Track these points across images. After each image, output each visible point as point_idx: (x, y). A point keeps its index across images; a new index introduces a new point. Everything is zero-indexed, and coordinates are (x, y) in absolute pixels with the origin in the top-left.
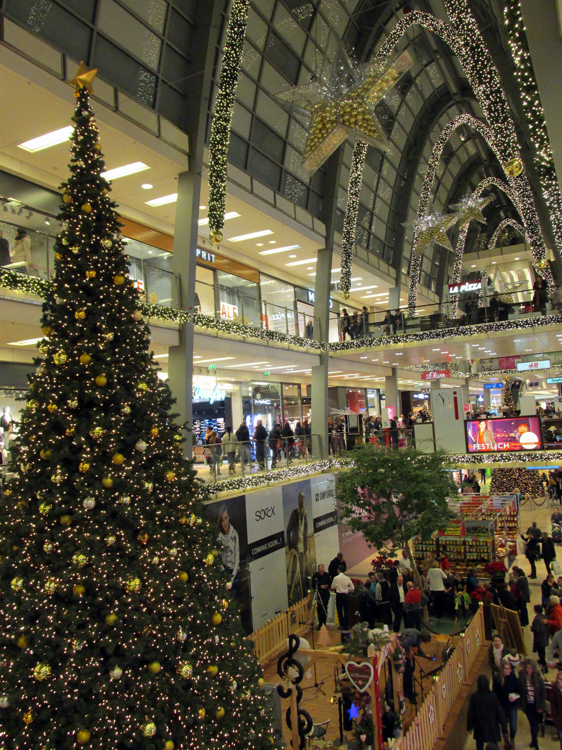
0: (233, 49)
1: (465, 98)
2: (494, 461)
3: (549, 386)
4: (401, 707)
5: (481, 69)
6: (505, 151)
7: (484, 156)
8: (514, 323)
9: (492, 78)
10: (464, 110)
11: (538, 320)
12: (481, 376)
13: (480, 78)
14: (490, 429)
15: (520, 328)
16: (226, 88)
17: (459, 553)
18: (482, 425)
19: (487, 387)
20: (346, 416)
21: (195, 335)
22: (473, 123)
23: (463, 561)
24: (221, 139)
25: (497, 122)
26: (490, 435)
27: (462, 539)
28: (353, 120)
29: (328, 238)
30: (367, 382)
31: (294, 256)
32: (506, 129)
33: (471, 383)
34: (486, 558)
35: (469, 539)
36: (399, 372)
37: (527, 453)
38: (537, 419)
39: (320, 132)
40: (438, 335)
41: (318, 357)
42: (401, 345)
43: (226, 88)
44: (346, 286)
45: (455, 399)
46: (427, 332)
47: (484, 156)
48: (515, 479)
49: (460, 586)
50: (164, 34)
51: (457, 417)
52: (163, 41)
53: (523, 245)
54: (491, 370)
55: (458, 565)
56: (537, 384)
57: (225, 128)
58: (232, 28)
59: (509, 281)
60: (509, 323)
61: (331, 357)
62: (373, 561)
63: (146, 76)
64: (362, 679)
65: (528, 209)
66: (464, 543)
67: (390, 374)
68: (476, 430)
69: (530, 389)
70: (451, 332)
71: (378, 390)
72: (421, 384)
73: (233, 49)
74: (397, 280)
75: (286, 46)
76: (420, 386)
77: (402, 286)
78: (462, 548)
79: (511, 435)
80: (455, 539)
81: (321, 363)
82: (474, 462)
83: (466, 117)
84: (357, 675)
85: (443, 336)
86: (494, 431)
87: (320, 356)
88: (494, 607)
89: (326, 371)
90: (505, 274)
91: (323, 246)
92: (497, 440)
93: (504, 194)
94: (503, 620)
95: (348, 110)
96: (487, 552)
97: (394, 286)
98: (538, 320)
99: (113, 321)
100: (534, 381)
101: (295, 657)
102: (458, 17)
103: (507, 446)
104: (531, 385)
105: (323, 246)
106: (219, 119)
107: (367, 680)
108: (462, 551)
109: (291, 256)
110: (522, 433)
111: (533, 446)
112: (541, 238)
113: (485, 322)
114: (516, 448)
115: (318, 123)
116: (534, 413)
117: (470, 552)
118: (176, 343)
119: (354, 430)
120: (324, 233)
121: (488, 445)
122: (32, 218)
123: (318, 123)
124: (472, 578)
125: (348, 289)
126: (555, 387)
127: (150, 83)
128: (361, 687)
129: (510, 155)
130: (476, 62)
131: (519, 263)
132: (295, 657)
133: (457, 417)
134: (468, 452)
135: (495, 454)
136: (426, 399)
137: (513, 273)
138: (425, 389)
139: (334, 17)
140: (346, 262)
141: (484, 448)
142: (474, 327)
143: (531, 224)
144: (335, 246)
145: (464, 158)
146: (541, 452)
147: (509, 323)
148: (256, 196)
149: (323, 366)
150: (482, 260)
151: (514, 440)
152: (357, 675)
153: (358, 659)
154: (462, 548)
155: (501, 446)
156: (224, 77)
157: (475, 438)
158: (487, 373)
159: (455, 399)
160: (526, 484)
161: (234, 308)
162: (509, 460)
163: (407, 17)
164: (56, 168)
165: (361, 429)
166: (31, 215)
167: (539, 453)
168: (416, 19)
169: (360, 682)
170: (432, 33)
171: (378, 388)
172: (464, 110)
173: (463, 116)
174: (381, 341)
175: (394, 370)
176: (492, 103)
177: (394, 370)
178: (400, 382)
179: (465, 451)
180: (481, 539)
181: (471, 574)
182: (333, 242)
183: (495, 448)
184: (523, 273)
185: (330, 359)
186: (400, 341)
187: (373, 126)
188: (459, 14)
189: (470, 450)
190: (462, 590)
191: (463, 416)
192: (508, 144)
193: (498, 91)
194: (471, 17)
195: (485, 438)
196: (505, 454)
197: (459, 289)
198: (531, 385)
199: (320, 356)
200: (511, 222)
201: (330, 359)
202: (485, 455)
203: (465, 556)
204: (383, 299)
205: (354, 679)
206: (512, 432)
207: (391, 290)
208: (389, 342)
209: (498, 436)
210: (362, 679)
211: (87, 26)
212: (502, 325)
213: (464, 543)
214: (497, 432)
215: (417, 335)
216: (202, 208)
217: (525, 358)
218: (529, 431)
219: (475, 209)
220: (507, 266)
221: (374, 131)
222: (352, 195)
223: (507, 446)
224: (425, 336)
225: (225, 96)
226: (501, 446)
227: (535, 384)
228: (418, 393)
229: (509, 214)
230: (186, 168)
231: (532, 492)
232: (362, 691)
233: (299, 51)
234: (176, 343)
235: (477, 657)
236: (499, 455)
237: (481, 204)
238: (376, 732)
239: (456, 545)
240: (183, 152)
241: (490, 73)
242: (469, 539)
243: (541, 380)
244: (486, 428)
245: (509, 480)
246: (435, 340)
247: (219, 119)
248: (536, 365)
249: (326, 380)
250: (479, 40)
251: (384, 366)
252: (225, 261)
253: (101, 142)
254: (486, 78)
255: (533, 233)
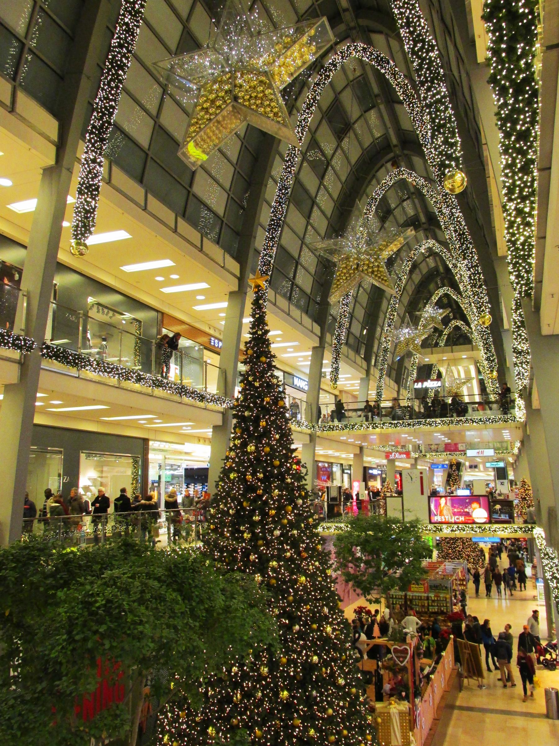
0: (280, 205)
1: (432, 227)
2: (452, 531)
3: (486, 469)
4: (420, 682)
5: (465, 249)
6: (480, 308)
7: (441, 269)
8: (471, 420)
9: (473, 257)
10: (430, 237)
11: (489, 419)
12: (428, 456)
13: (464, 255)
14: (449, 504)
15: (475, 424)
16: (272, 233)
17: (423, 606)
18: (443, 501)
19: (433, 466)
20: (328, 488)
21: (41, 371)
22: (437, 248)
23: (426, 613)
24: (266, 270)
25: (475, 287)
26: (449, 510)
27: (426, 595)
28: (370, 270)
29: (322, 339)
30: (343, 459)
31: (292, 350)
32: (481, 293)
33: (419, 462)
34: (445, 611)
35: (432, 595)
36: (365, 451)
37: (478, 525)
38: (486, 498)
39: (345, 275)
40: (409, 425)
41: (221, 415)
42: (378, 430)
43: (272, 233)
44: (335, 379)
45: (422, 478)
46: (401, 421)
47: (441, 269)
48: (459, 551)
49: (426, 631)
50: (230, 190)
51: (422, 493)
52: (229, 195)
53: (470, 346)
54: (437, 452)
55: (422, 616)
56: (476, 467)
57: (270, 262)
58: (280, 190)
59: (456, 376)
60: (467, 420)
61: (318, 436)
62: (355, 610)
63: (206, 214)
64: (402, 657)
65: (485, 331)
66: (428, 598)
67: (358, 451)
68: (438, 505)
69: (469, 470)
70: (420, 423)
71: (342, 465)
72: (377, 461)
73: (280, 205)
74: (368, 372)
75: (306, 191)
76: (377, 463)
77: (371, 377)
78: (426, 602)
79: (466, 510)
80: (420, 595)
81: (311, 441)
82: (435, 531)
83: (431, 243)
84: (399, 655)
85: (413, 426)
86: (452, 506)
87: (310, 435)
88: (460, 642)
89: (315, 447)
90: (453, 368)
91: (317, 345)
92: (454, 514)
93: (457, 303)
94: (467, 651)
95: (367, 262)
96: (446, 606)
97: (364, 376)
98: (489, 419)
99: (278, 428)
100: (473, 464)
101: (357, 645)
102: (451, 211)
103: (462, 519)
104: (471, 467)
105: (317, 345)
106: (266, 255)
107: (406, 658)
108: (426, 605)
109: (289, 350)
110: (474, 509)
111: (483, 520)
112: (493, 355)
113: (447, 417)
114: (469, 521)
115: (343, 268)
116: (484, 493)
117: (432, 606)
118: (220, 423)
119: (334, 499)
120: (319, 334)
121: (447, 517)
122: (113, 318)
123: (343, 268)
124: (436, 626)
125: (336, 382)
126: (491, 470)
127: (209, 219)
128: (402, 662)
129: (483, 311)
130: (462, 244)
131: (466, 360)
132: (357, 645)
133: (422, 493)
134: (431, 522)
135: (452, 525)
136: (379, 474)
137: (461, 368)
138: (380, 466)
139: (337, 163)
140: (336, 359)
141: (443, 520)
142: (438, 420)
143: (487, 344)
144: (326, 345)
145: (425, 271)
146: (489, 525)
147: (467, 420)
148: (291, 317)
149: (312, 444)
150: (434, 355)
151: (468, 514)
152: (399, 655)
153: (400, 644)
154: (426, 602)
155: (458, 519)
156: (272, 224)
157: (437, 511)
158: (434, 454)
159: (422, 478)
160: (469, 556)
161: (176, 369)
162: (464, 530)
163: (395, 171)
164: (137, 282)
165: (340, 499)
166: (114, 315)
167: (487, 526)
168: (403, 174)
169: (401, 659)
170: (414, 186)
171: (342, 462)
172: (430, 237)
173: (429, 241)
174: (362, 426)
175: (361, 448)
176: (472, 274)
177: (361, 448)
178: (366, 459)
179: (428, 522)
180: (441, 595)
181: (436, 622)
182: (325, 342)
183: (453, 521)
184: (468, 367)
185: (317, 439)
186: (377, 427)
187: (385, 276)
188: (451, 209)
189: (433, 521)
190: (428, 635)
191: (427, 492)
192: (482, 303)
193: (476, 266)
194: (460, 212)
195: (445, 512)
196: (460, 526)
197: (422, 384)
198: (471, 467)
199: (310, 435)
200: (459, 323)
201: (317, 439)
202: (444, 526)
203: (428, 610)
204: (353, 385)
205: (397, 657)
206: (466, 508)
207: (362, 379)
208: (368, 428)
209: (455, 510)
210: (402, 657)
211: (186, 188)
212: (461, 420)
213: (428, 598)
214: (455, 507)
215: (392, 424)
216: (65, 224)
217: (472, 446)
218: (480, 507)
219: (436, 318)
220: (456, 361)
221: (386, 281)
222: (343, 305)
223: (462, 519)
224: (398, 425)
225: (271, 238)
226: (458, 519)
227: (474, 467)
228: (372, 468)
229: (458, 316)
230: (236, 289)
231: (473, 563)
232: (402, 665)
233: (313, 194)
234: (220, 423)
235: (450, 675)
236: (456, 526)
237: (441, 315)
238: (411, 691)
239: (421, 599)
240: (235, 276)
241: (471, 253)
242: (432, 595)
243: (479, 462)
244: (446, 503)
245: (454, 552)
246: (407, 429)
247: (266, 255)
248: (482, 453)
249: (314, 455)
250: (464, 229)
251: (355, 445)
252: (184, 327)
253: (267, 318)
254: (468, 256)
255: (488, 350)
